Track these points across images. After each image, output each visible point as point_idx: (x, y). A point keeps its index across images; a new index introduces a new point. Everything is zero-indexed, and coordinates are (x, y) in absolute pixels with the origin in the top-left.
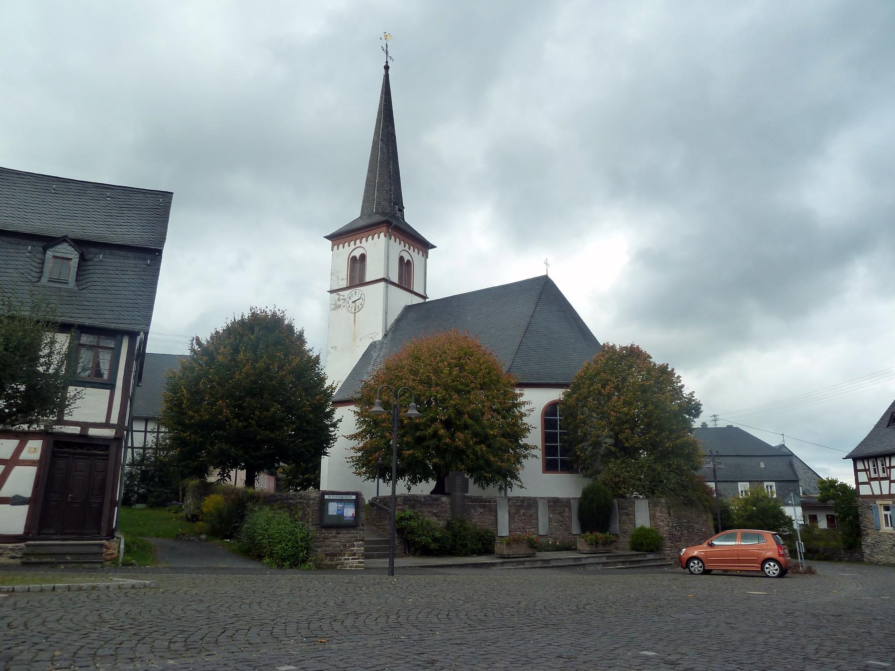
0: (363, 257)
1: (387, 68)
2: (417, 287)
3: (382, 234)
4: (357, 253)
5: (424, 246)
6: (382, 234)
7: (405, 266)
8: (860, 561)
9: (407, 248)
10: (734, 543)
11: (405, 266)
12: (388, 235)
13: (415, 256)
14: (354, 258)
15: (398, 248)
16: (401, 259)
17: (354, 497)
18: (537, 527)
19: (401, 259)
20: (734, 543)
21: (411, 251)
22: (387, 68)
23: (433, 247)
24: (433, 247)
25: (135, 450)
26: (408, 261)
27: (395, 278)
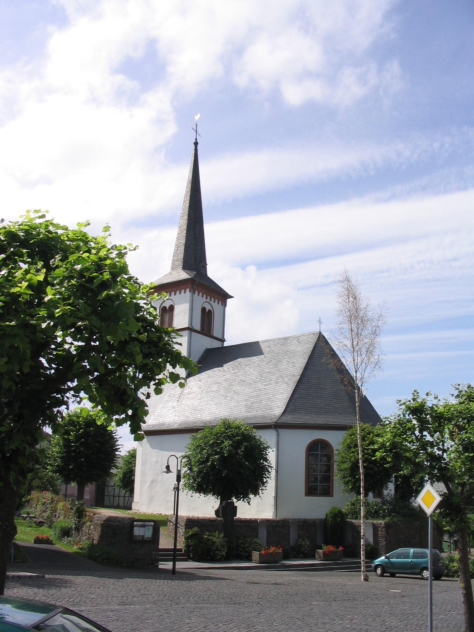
0: (172, 308)
1: (196, 144)
2: (216, 333)
3: (188, 290)
4: (167, 305)
5: (222, 296)
6: (188, 290)
7: (207, 317)
8: (432, 485)
9: (208, 300)
10: (13, 573)
11: (207, 317)
12: (193, 291)
13: (216, 306)
14: (164, 308)
15: (201, 300)
16: (204, 309)
17: (385, 574)
18: (289, 540)
19: (204, 309)
20: (13, 573)
21: (212, 302)
22: (196, 144)
23: (231, 297)
24: (231, 297)
25: (118, 498)
26: (210, 311)
27: (198, 327)
